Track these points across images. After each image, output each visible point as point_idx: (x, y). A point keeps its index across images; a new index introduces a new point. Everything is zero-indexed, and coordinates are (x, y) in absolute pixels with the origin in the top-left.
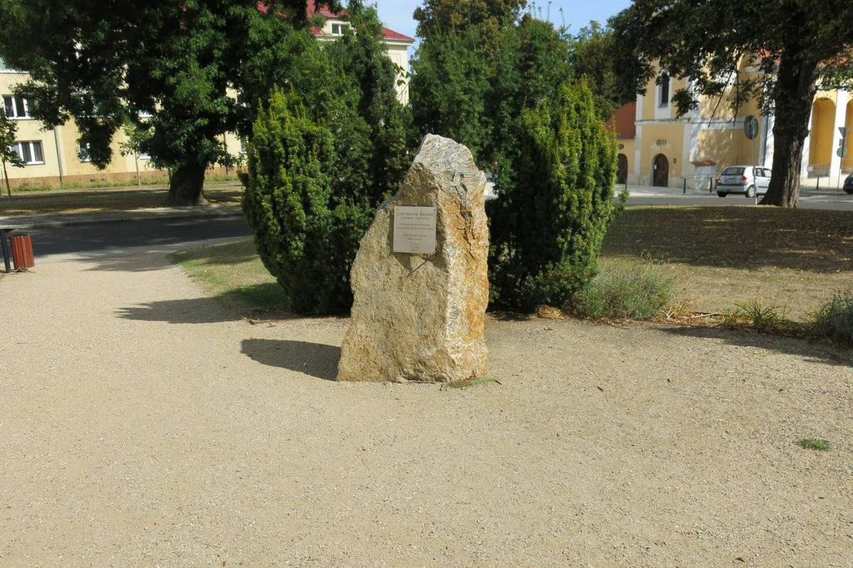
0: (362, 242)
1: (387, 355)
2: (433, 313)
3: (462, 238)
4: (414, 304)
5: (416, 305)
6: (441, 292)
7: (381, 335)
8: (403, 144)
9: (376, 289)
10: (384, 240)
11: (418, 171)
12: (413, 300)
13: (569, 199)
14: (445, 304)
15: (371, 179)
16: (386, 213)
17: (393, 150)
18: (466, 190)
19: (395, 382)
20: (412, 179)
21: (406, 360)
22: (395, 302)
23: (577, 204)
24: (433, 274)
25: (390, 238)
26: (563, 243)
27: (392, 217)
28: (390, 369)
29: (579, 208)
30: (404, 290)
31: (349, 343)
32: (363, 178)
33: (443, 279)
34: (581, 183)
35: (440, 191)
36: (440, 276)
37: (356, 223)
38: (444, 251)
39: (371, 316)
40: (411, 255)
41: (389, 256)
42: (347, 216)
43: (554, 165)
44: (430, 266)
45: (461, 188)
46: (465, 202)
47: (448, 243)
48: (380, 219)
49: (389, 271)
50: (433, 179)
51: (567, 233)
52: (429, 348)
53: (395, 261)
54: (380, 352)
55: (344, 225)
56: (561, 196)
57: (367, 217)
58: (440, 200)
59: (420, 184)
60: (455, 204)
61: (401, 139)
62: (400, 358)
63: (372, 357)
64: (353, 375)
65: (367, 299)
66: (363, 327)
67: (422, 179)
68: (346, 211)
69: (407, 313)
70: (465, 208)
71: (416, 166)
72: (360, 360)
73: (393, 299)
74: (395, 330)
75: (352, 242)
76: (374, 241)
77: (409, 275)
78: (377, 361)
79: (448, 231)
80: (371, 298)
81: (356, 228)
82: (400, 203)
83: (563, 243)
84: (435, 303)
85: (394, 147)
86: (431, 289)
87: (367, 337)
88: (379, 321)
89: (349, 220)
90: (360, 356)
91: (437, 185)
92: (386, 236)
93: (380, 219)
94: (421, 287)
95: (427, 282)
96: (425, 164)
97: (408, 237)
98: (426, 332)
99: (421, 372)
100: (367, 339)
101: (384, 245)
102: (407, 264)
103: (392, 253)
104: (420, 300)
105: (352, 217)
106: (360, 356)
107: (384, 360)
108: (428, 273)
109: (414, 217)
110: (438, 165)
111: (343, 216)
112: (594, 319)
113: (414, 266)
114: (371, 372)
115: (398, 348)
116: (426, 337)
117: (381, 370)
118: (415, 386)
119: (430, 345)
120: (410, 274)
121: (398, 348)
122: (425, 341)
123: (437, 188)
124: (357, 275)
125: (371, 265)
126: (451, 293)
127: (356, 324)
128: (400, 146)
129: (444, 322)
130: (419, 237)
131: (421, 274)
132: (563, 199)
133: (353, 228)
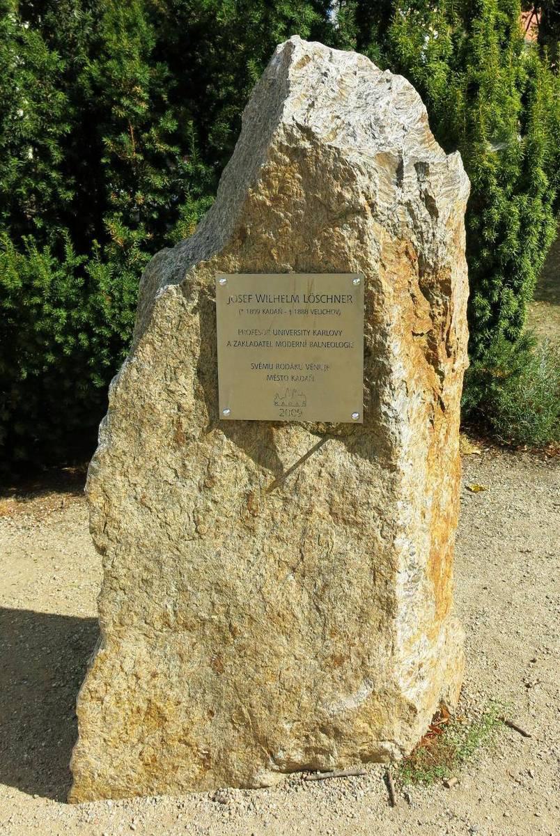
0: (116, 392)
1: (220, 720)
2: (356, 593)
3: (423, 359)
4: (294, 570)
5: (301, 571)
6: (374, 526)
7: (198, 665)
8: (141, 99)
9: (173, 535)
10: (187, 383)
11: (297, 153)
12: (291, 555)
13: (503, 217)
14: (389, 560)
15: (68, 188)
16: (187, 295)
17: (122, 114)
18: (433, 211)
19: (250, 787)
20: (275, 183)
21: (282, 731)
22: (234, 568)
23: (516, 227)
24: (347, 478)
25: (207, 375)
26: (483, 309)
27: (208, 311)
28: (233, 756)
29: (523, 235)
30: (261, 530)
31: (101, 700)
32: (50, 184)
33: (379, 486)
34: (525, 185)
35: (371, 221)
36: (370, 482)
37: (47, 294)
38: (384, 408)
39: (165, 616)
40: (278, 425)
41: (205, 432)
42: (21, 277)
43: (475, 144)
44: (338, 456)
45: (422, 205)
46: (435, 252)
47: (396, 384)
48: (168, 319)
49: (211, 477)
50: (349, 178)
51: (493, 286)
52: (349, 689)
53: (227, 445)
54: (198, 713)
55: (16, 300)
56: (485, 211)
57: (70, 278)
58: (372, 248)
59: (301, 200)
60: (405, 259)
61: (138, 89)
62: (265, 727)
63: (175, 728)
64: (121, 784)
65: (146, 569)
66: (142, 649)
67: (311, 183)
68: (18, 267)
69: (275, 595)
70: (435, 271)
71: (290, 137)
72: (141, 740)
73: (230, 559)
74: (241, 648)
75: (39, 341)
76: (155, 389)
77: (273, 486)
78: (192, 737)
79: (396, 345)
80: (158, 562)
81: (47, 308)
82: (234, 262)
83: (483, 309)
84: (358, 560)
85: (121, 106)
86: (346, 522)
87: (154, 675)
88: (188, 627)
89: (28, 289)
90: (138, 729)
91: (362, 200)
92: (192, 371)
93: (168, 319)
94: (314, 519)
95: (331, 503)
96: (322, 133)
97: (266, 372)
98: (340, 647)
99: (327, 752)
100: (159, 681)
101: (189, 401)
102: (265, 453)
103: (215, 422)
104: (314, 555)
105: (36, 283)
106: (138, 729)
107: (209, 735)
108: (332, 475)
109: (287, 307)
110: (354, 135)
111: (12, 279)
112: (539, 450)
113: (288, 458)
114: (175, 768)
115: (256, 699)
116: (339, 661)
117: (205, 761)
118: (309, 795)
119: (352, 681)
120: (279, 482)
121: (256, 699)
122: (337, 672)
123: (362, 212)
124: (108, 499)
125: (150, 465)
126: (403, 529)
127: (118, 644)
128: (135, 105)
129: (389, 612)
130: (304, 373)
131: (311, 479)
132: (490, 218)
133: (40, 306)
